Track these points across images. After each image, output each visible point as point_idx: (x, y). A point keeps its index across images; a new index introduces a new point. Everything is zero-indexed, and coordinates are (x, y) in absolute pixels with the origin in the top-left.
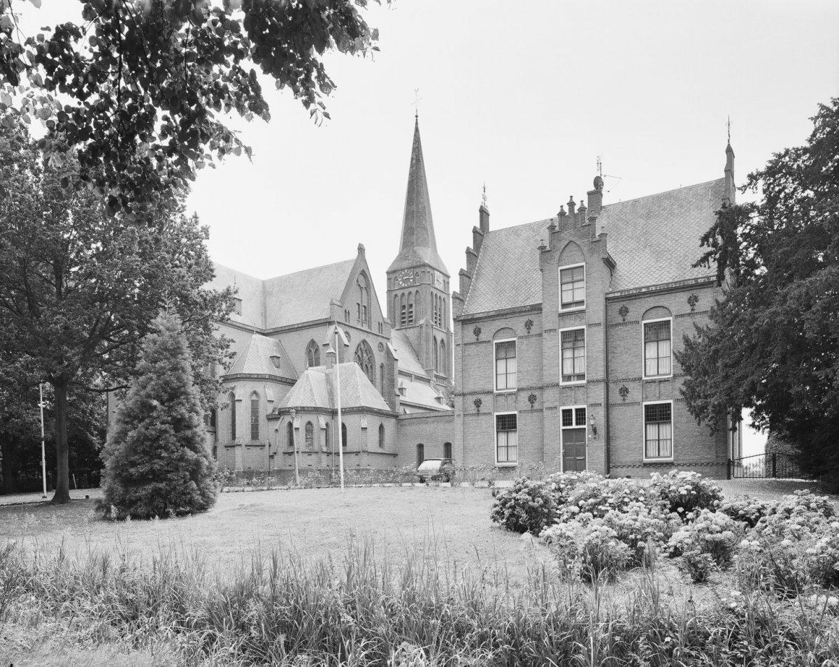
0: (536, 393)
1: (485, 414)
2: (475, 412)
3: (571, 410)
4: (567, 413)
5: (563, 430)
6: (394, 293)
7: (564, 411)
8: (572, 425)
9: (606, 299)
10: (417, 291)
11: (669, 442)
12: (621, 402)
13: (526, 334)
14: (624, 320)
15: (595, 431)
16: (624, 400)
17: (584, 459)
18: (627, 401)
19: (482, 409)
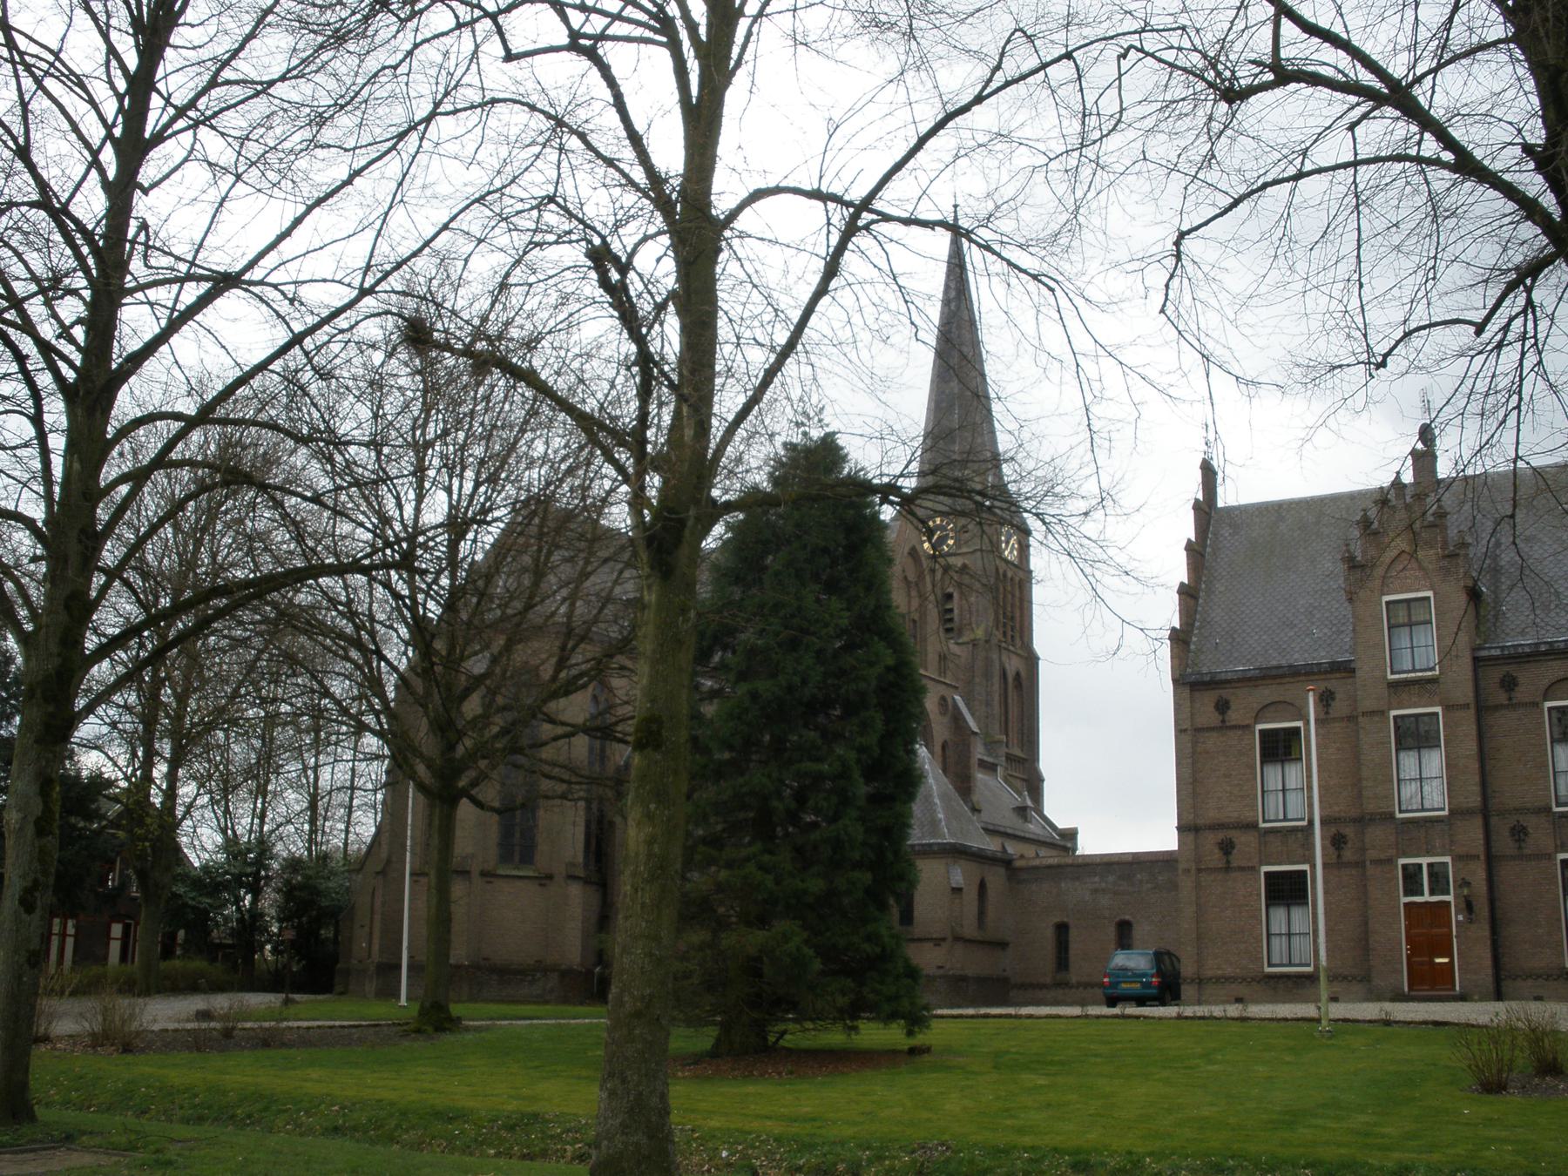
1: (1242, 869)
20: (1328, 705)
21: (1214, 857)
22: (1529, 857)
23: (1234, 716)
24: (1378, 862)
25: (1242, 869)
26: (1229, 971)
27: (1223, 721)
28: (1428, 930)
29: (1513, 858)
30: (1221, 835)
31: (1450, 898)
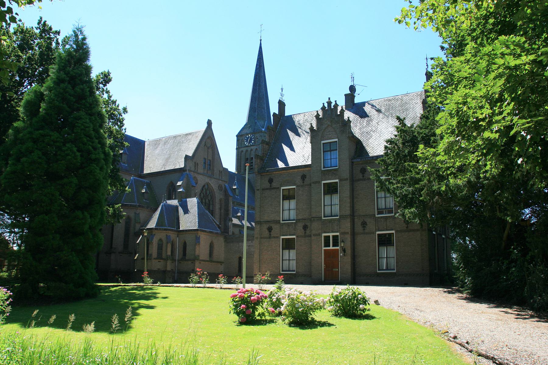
0: (308, 224)
1: (274, 237)
2: (268, 235)
4: (327, 239)
6: (241, 149)
10: (256, 149)
13: (302, 184)
16: (364, 229)
18: (366, 231)
19: (273, 233)
20: (304, 180)
22: (367, 233)
23: (274, 185)
24: (315, 235)
25: (274, 237)
31: (324, 248)
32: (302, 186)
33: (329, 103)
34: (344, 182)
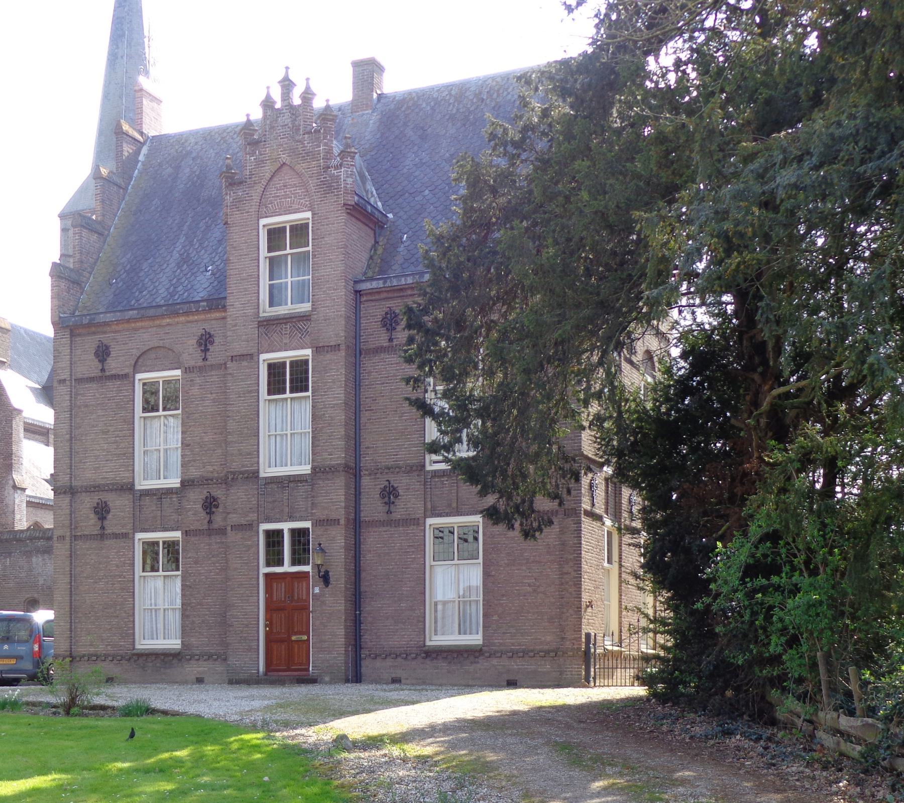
0: (218, 492)
1: (116, 536)
2: (96, 531)
3: (282, 530)
4: (274, 538)
5: (267, 576)
7: (269, 534)
8: (283, 565)
9: (358, 293)
11: (474, 607)
12: (382, 517)
13: (200, 363)
14: (391, 340)
15: (325, 579)
16: (389, 512)
17: (308, 640)
18: (396, 516)
19: (112, 526)
20: (206, 350)
21: (90, 524)
22: (397, 523)
23: (114, 365)
25: (116, 536)
26: (101, 649)
27: (103, 370)
28: (287, 608)
29: (383, 523)
30: (95, 498)
32: (201, 369)
33: (287, 85)
34: (328, 356)
